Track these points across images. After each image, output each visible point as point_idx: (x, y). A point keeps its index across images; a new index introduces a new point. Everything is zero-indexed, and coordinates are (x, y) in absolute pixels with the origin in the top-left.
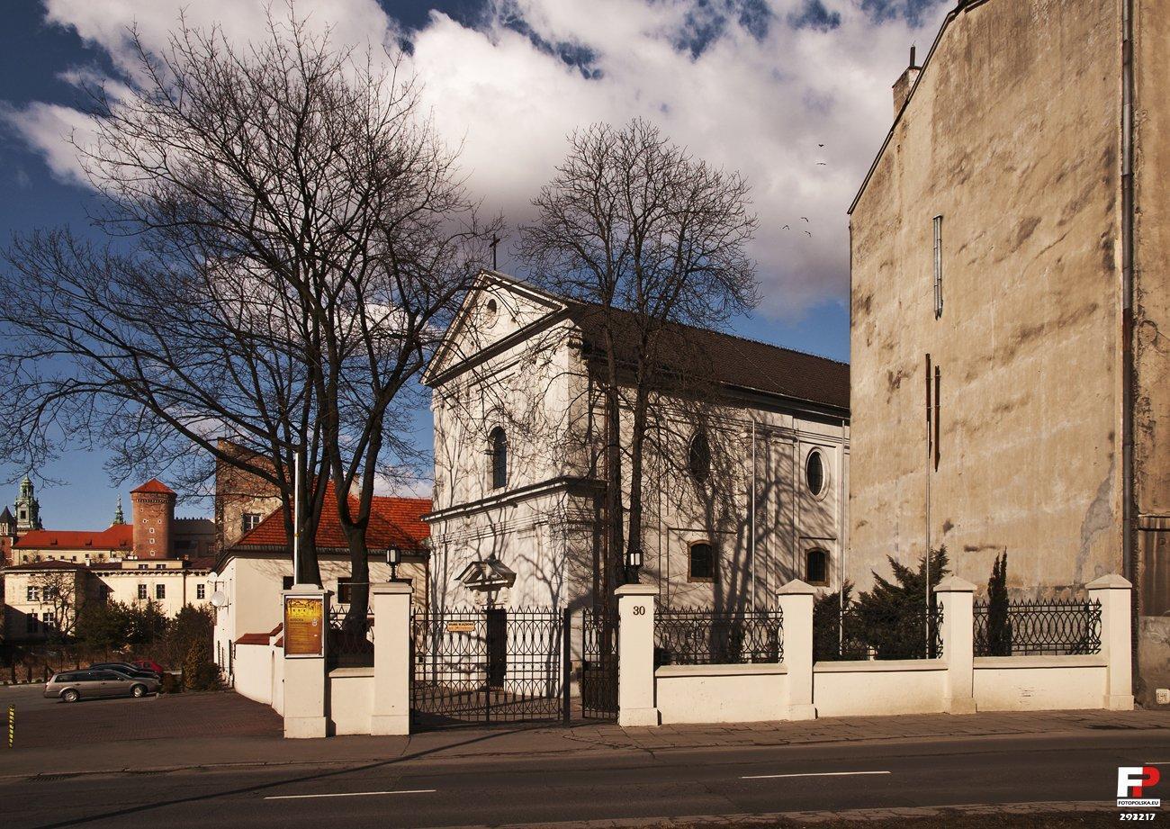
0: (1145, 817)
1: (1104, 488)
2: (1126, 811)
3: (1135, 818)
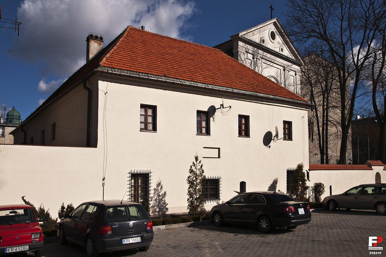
0: (376, 253)
3: (375, 253)
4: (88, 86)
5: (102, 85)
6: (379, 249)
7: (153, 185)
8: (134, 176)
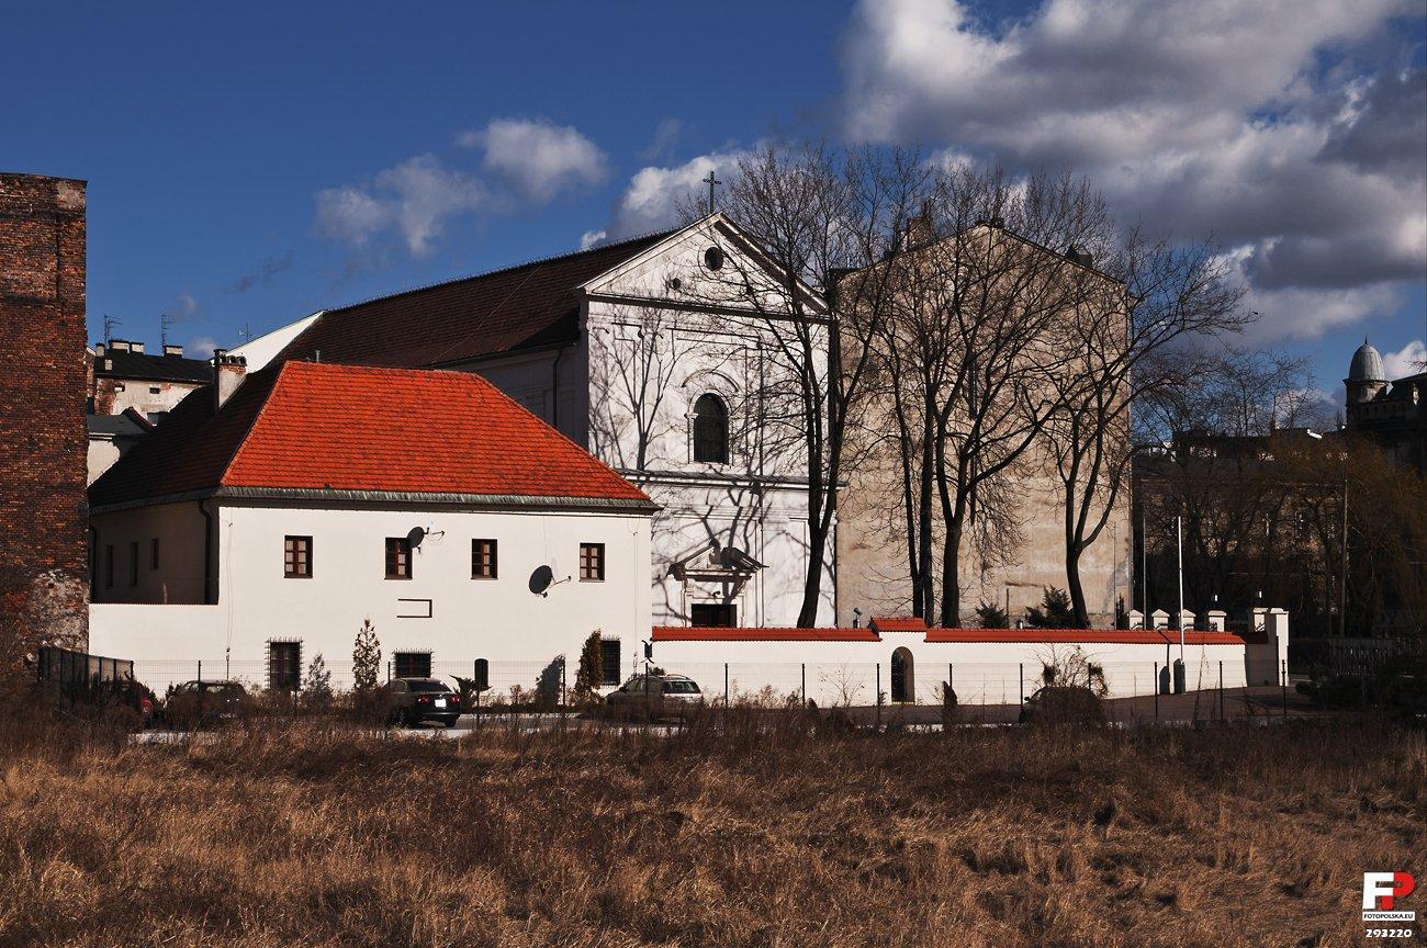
0: (1389, 933)
1: (1122, 565)
2: (1371, 925)
3: (1385, 935)
4: (206, 508)
5: (225, 513)
6: (1401, 919)
7: (307, 658)
8: (276, 646)
